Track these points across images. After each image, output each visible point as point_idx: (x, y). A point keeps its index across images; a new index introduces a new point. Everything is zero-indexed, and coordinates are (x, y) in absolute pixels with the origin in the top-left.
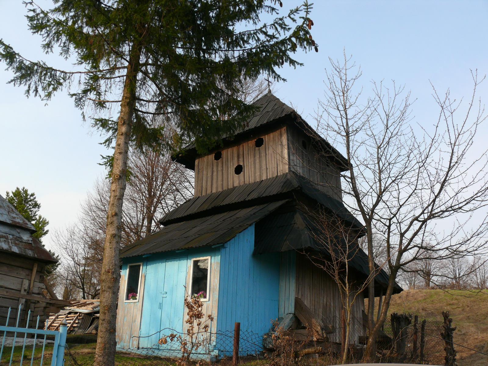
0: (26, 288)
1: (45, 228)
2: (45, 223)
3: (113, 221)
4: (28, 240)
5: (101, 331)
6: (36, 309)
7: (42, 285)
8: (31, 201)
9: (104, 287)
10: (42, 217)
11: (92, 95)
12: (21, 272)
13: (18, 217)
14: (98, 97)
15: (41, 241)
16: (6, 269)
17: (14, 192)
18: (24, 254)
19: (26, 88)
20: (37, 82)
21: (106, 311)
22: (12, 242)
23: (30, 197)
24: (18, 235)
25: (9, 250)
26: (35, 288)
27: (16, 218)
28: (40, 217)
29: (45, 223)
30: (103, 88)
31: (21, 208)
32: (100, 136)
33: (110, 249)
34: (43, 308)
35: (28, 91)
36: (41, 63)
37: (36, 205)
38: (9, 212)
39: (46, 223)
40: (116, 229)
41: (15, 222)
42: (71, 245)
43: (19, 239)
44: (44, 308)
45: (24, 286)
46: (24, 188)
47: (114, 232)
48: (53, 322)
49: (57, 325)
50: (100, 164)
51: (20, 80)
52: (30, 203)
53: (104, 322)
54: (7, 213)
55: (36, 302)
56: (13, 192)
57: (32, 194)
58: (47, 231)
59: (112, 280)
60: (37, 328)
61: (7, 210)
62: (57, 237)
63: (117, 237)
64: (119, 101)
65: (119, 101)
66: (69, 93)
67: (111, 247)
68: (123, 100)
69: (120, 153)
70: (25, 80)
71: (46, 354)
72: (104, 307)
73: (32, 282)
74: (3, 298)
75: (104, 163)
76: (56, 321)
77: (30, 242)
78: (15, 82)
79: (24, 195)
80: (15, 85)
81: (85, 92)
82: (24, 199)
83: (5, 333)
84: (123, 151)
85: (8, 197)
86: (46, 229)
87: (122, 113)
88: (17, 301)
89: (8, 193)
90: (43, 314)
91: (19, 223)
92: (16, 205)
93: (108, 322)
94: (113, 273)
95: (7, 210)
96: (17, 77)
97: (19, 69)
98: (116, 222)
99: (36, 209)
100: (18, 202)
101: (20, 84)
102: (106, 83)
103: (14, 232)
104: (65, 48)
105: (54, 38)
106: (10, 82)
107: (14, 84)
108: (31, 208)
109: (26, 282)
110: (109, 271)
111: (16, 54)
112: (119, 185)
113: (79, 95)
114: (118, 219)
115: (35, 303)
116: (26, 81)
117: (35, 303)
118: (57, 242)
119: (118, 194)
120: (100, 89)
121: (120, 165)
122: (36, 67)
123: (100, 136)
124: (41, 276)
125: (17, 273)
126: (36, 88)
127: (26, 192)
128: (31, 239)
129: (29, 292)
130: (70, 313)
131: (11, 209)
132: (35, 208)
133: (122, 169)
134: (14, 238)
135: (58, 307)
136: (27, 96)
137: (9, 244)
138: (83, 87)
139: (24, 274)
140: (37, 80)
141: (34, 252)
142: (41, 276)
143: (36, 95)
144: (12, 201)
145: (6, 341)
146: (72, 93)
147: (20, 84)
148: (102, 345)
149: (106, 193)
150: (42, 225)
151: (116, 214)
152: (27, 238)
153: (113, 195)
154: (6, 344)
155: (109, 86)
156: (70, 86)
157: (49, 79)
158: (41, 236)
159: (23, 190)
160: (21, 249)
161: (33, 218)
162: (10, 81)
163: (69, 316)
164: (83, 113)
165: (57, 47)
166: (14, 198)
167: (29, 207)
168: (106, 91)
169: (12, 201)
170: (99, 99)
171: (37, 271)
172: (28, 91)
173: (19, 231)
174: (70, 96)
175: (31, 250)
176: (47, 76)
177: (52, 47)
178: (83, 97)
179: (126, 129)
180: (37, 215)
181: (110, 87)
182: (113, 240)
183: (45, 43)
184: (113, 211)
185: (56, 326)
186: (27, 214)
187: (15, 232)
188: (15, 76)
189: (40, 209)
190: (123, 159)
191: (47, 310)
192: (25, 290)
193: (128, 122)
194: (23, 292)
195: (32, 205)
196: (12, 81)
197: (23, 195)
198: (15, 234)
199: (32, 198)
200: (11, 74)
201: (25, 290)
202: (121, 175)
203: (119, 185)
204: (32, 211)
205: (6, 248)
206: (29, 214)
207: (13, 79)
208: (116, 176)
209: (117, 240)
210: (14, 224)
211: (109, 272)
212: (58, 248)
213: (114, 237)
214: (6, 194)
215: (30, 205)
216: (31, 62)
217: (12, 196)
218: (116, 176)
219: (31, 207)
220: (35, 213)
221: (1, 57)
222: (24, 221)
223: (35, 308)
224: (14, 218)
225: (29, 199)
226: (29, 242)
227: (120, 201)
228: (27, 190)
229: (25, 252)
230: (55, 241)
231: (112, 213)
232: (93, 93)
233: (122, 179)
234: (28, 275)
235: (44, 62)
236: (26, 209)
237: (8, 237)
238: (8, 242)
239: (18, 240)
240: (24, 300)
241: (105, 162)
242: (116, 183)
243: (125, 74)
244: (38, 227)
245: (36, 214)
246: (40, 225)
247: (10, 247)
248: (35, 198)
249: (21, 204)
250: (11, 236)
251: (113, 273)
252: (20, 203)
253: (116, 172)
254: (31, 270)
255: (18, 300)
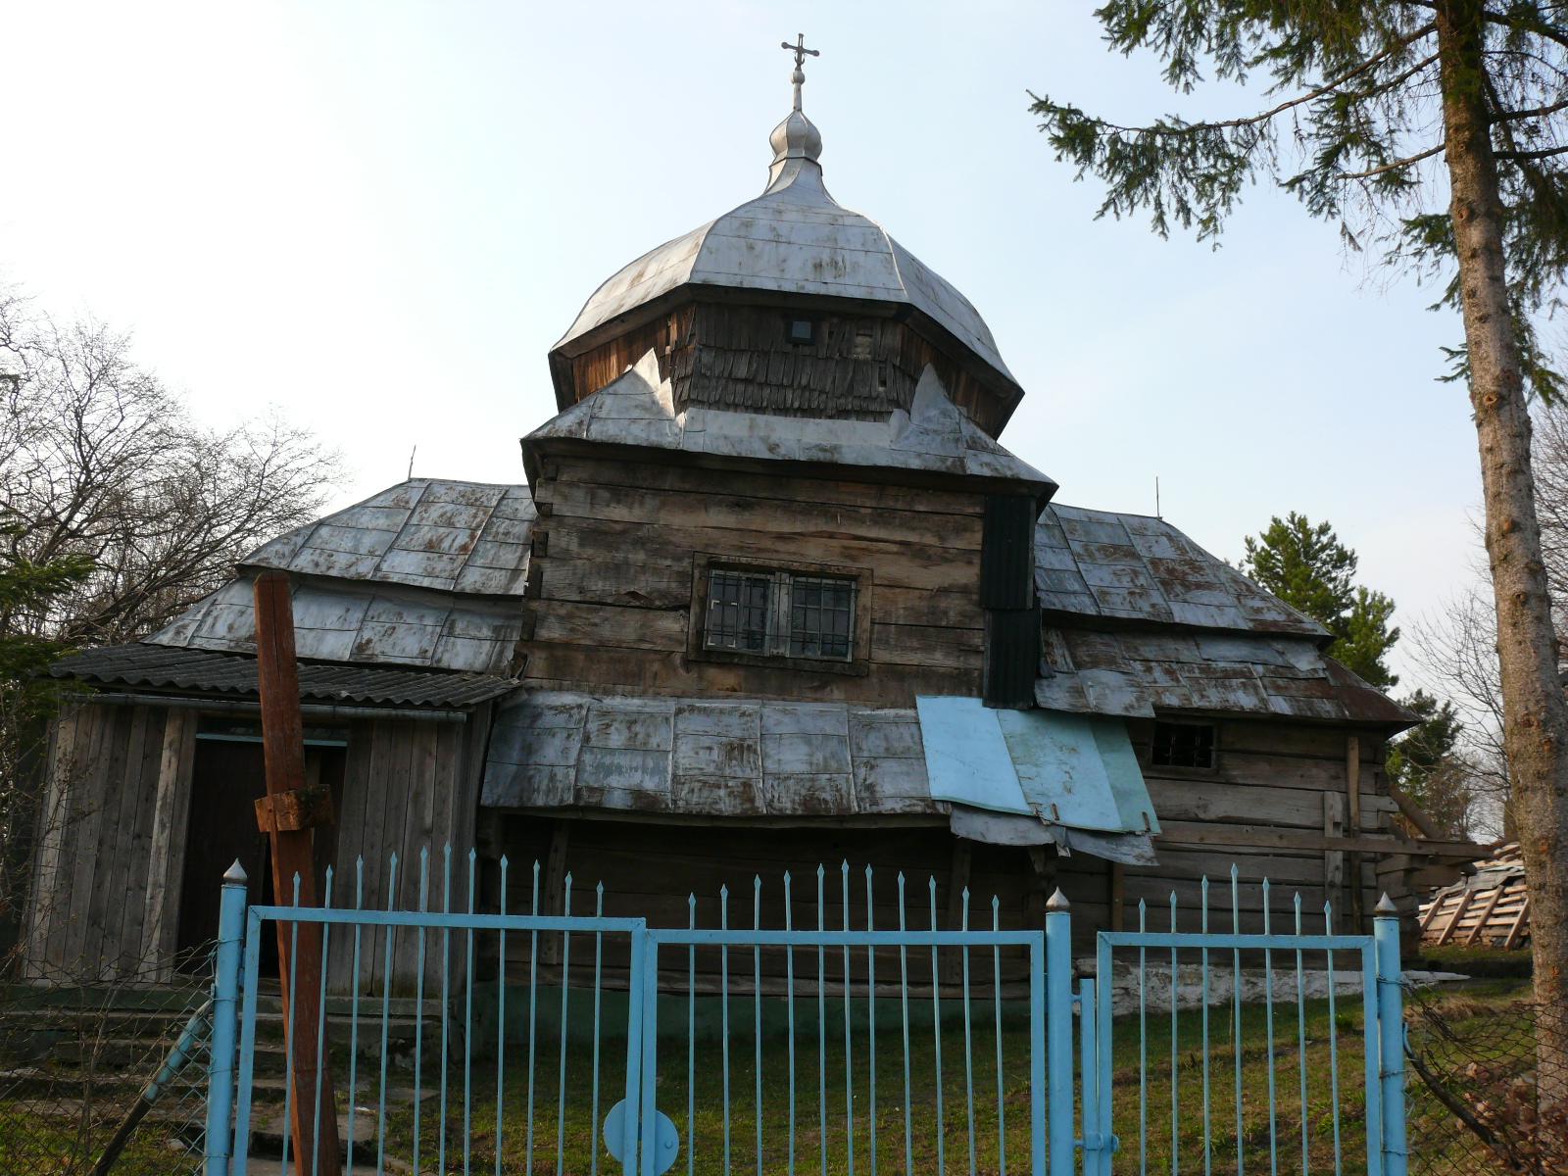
0: (1338, 819)
1: (1386, 622)
2: (1384, 608)
3: (1511, 552)
4: (1315, 670)
5: (1538, 927)
6: (1381, 878)
7: (1385, 803)
8: (1323, 548)
9: (1524, 775)
10: (1370, 591)
11: (1355, 162)
12: (1314, 771)
13: (1270, 605)
14: (1374, 158)
15: (1385, 666)
16: (1268, 767)
17: (1267, 533)
18: (1309, 714)
19: (1151, 212)
20: (1178, 184)
21: (1543, 857)
22: (1267, 683)
23: (1319, 537)
24: (1280, 661)
25: (1262, 711)
26: (1365, 814)
27: (1265, 611)
28: (1364, 593)
29: (1384, 608)
30: (1380, 127)
31: (1301, 576)
32: (1419, 284)
33: (1518, 648)
34: (1402, 873)
35: (1160, 219)
36: (1169, 123)
37: (1344, 559)
38: (1238, 596)
39: (1384, 608)
40: (1525, 577)
41: (1262, 622)
42: (1473, 661)
43: (1287, 672)
44: (1405, 876)
45: (1331, 813)
46: (1293, 515)
47: (1519, 587)
48: (1460, 917)
49: (1475, 923)
50: (1446, 379)
51: (1128, 196)
52: (1324, 556)
53: (1543, 894)
54: (1236, 602)
55: (1379, 857)
56: (1263, 536)
57: (1321, 527)
58: (1396, 632)
59: (1546, 748)
60: (1173, 929)
61: (1232, 591)
62: (1423, 641)
63: (1533, 602)
64: (1440, 149)
65: (1440, 149)
66: (1278, 180)
67: (1519, 637)
68: (1450, 141)
69: (1483, 319)
70: (1140, 191)
71: (1411, 1016)
72: (1534, 843)
73: (1353, 796)
74: (1275, 855)
75: (1460, 369)
76: (1469, 911)
77: (1322, 675)
78: (1116, 208)
79: (1300, 536)
80: (1118, 214)
81: (1329, 159)
82: (1303, 546)
83: (1143, 951)
84: (1491, 310)
85: (1253, 554)
86: (1390, 625)
87: (1458, 185)
88: (1318, 862)
89: (1249, 542)
90: (1403, 891)
91: (1275, 623)
92: (1281, 573)
93: (1557, 891)
94: (1544, 725)
95: (1232, 591)
96: (1115, 190)
97: (1116, 160)
98: (1519, 551)
99: (1346, 571)
100: (1287, 561)
101: (1132, 204)
102: (1386, 106)
103: (1266, 654)
104: (1228, 50)
105: (1186, 34)
106: (1102, 214)
107: (1116, 212)
108: (1329, 572)
109: (1335, 801)
110: (1528, 720)
111: (1094, 124)
112: (1503, 427)
113: (1314, 176)
114: (1524, 540)
115: (1374, 861)
116: (1146, 190)
117: (1374, 861)
118: (1424, 659)
119: (1505, 456)
120: (1375, 133)
121: (1492, 359)
122: (1159, 141)
123: (1419, 284)
124: (1377, 774)
125: (1302, 776)
126: (1180, 200)
127: (1302, 524)
128: (1321, 665)
129: (1349, 829)
130: (1509, 882)
131: (1244, 587)
132: (1341, 567)
133: (1503, 370)
134: (1268, 670)
135: (1453, 866)
136: (1163, 233)
137: (1257, 693)
138: (1315, 149)
139: (1323, 775)
140: (1176, 178)
141: (1337, 705)
142: (1377, 774)
143: (1188, 222)
144: (1267, 561)
145: (1308, 982)
146: (1286, 178)
147: (1132, 204)
148: (1549, 974)
149: (1549, 466)
150: (1374, 616)
151: (1514, 527)
152: (1310, 663)
153: (1489, 465)
154: (1311, 991)
155: (1396, 109)
156: (1275, 159)
157: (1207, 159)
158: (1379, 653)
159: (1293, 522)
160: (1297, 701)
161: (1344, 601)
162: (1100, 208)
163: (1508, 890)
164: (1344, 226)
165: (1205, 60)
166: (1273, 552)
167: (1324, 569)
168: (1391, 132)
169: (1267, 561)
170: (1383, 162)
171: (1361, 761)
172: (1160, 219)
173: (1279, 646)
174: (1286, 189)
175: (1329, 698)
176: (1199, 154)
177: (1192, 63)
178: (1325, 177)
179: (1482, 232)
180: (1352, 589)
181: (1400, 114)
182: (1522, 615)
183: (1168, 62)
184: (1502, 518)
185: (1471, 928)
186: (1319, 592)
187: (1268, 654)
188: (1111, 187)
189: (1359, 566)
190: (1498, 336)
191: (1417, 877)
192: (1336, 825)
193: (1482, 209)
194: (1330, 831)
195: (1331, 560)
196: (1106, 206)
197: (1296, 536)
198: (1271, 660)
199: (1324, 539)
200: (1097, 185)
201: (1336, 825)
202: (1505, 392)
203: (1503, 427)
204: (1335, 579)
205: (1251, 706)
206: (1327, 589)
207: (1105, 199)
208: (1485, 399)
209: (1536, 614)
210: (1260, 628)
211: (1528, 724)
212: (1435, 679)
213: (1524, 604)
214: (1246, 545)
215: (1324, 563)
216: (1141, 131)
217: (1263, 549)
218: (1485, 399)
219: (1329, 567)
220: (1347, 582)
221: (1057, 149)
222: (1289, 614)
223: (1377, 875)
224: (1258, 610)
225: (1316, 543)
226: (1316, 676)
227: (1520, 478)
228: (1305, 519)
229: (1310, 709)
230: (1419, 658)
231: (1500, 527)
232: (1357, 154)
233: (1509, 404)
234: (1336, 778)
235: (1174, 116)
236: (1316, 578)
237: (1251, 673)
238: (1255, 687)
239: (1283, 677)
240: (1339, 855)
241: (1462, 365)
242: (1489, 423)
243: (1435, 51)
244: (1366, 622)
245: (1349, 587)
246: (1371, 617)
247: (1262, 700)
248: (1334, 538)
249: (1297, 565)
250: (1260, 669)
251: (1544, 725)
252: (1292, 562)
253: (1483, 387)
254: (1343, 760)
255: (1322, 858)
